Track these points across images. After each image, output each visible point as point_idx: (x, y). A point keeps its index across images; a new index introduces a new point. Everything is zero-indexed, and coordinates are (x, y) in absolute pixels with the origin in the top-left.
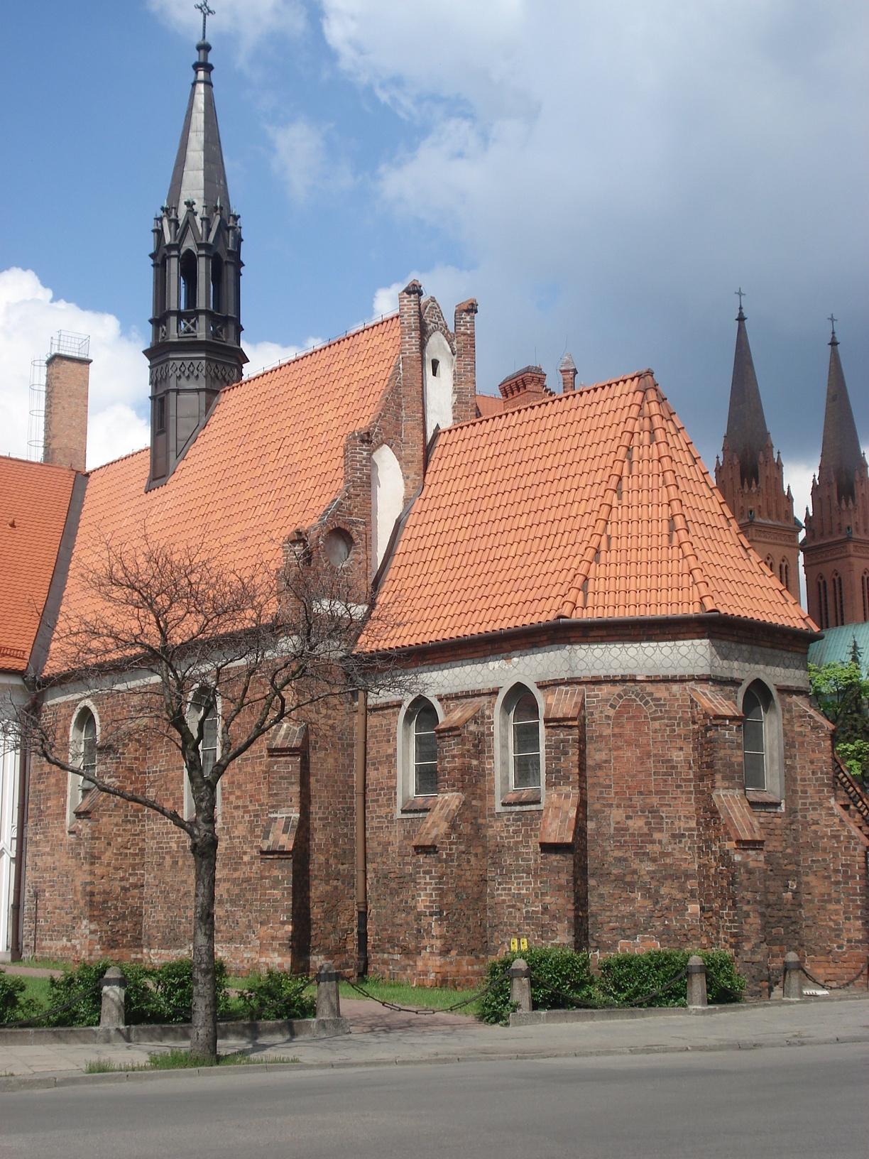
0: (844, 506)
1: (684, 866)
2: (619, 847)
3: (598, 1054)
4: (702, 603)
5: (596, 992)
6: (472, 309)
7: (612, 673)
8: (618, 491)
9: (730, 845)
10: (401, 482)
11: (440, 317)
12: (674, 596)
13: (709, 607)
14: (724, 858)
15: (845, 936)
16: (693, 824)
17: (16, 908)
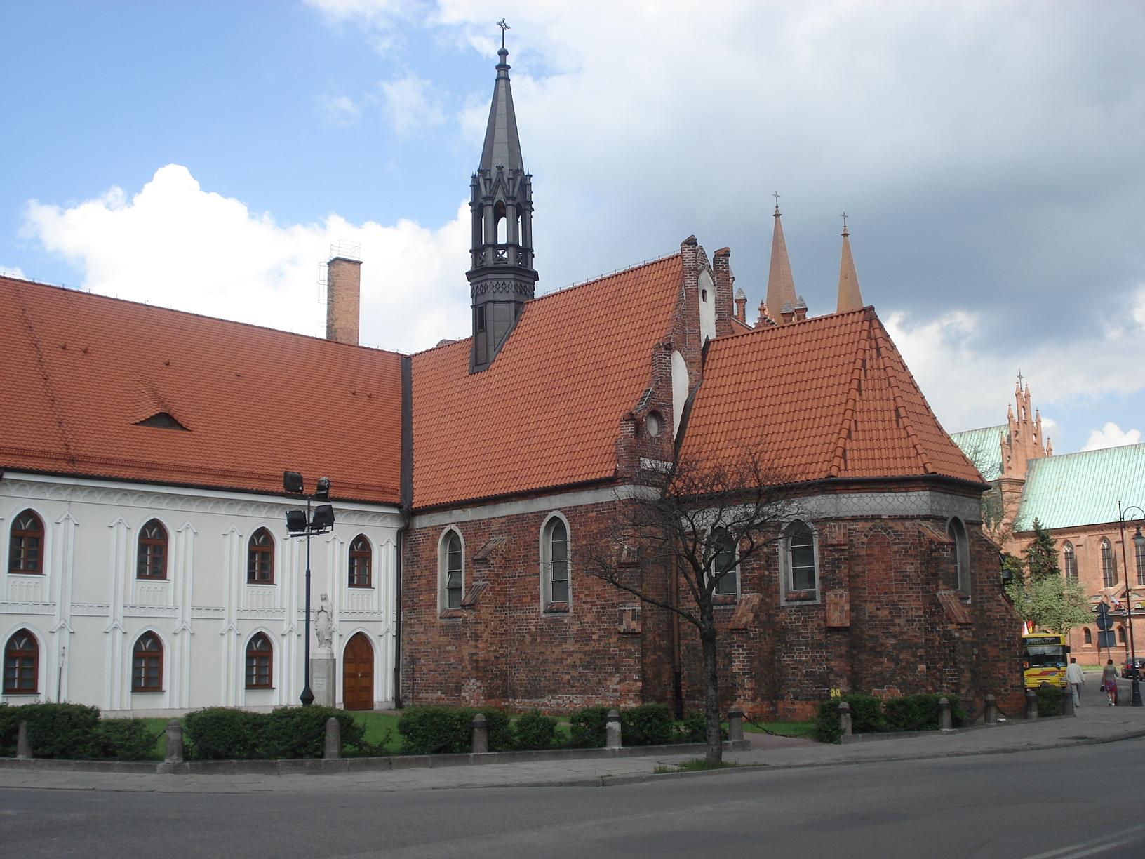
1: (915, 640)
2: (872, 629)
3: (931, 757)
4: (925, 468)
5: (883, 723)
6: (726, 253)
7: (865, 513)
8: (859, 390)
9: (950, 627)
11: (706, 260)
14: (947, 635)
15: (1009, 683)
16: (921, 613)
17: (397, 670)
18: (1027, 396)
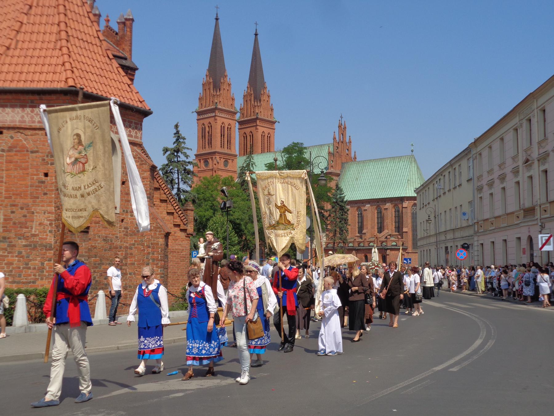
0: (256, 104)
10: (143, 124)
12: (50, 77)
13: (71, 82)
18: (345, 128)
